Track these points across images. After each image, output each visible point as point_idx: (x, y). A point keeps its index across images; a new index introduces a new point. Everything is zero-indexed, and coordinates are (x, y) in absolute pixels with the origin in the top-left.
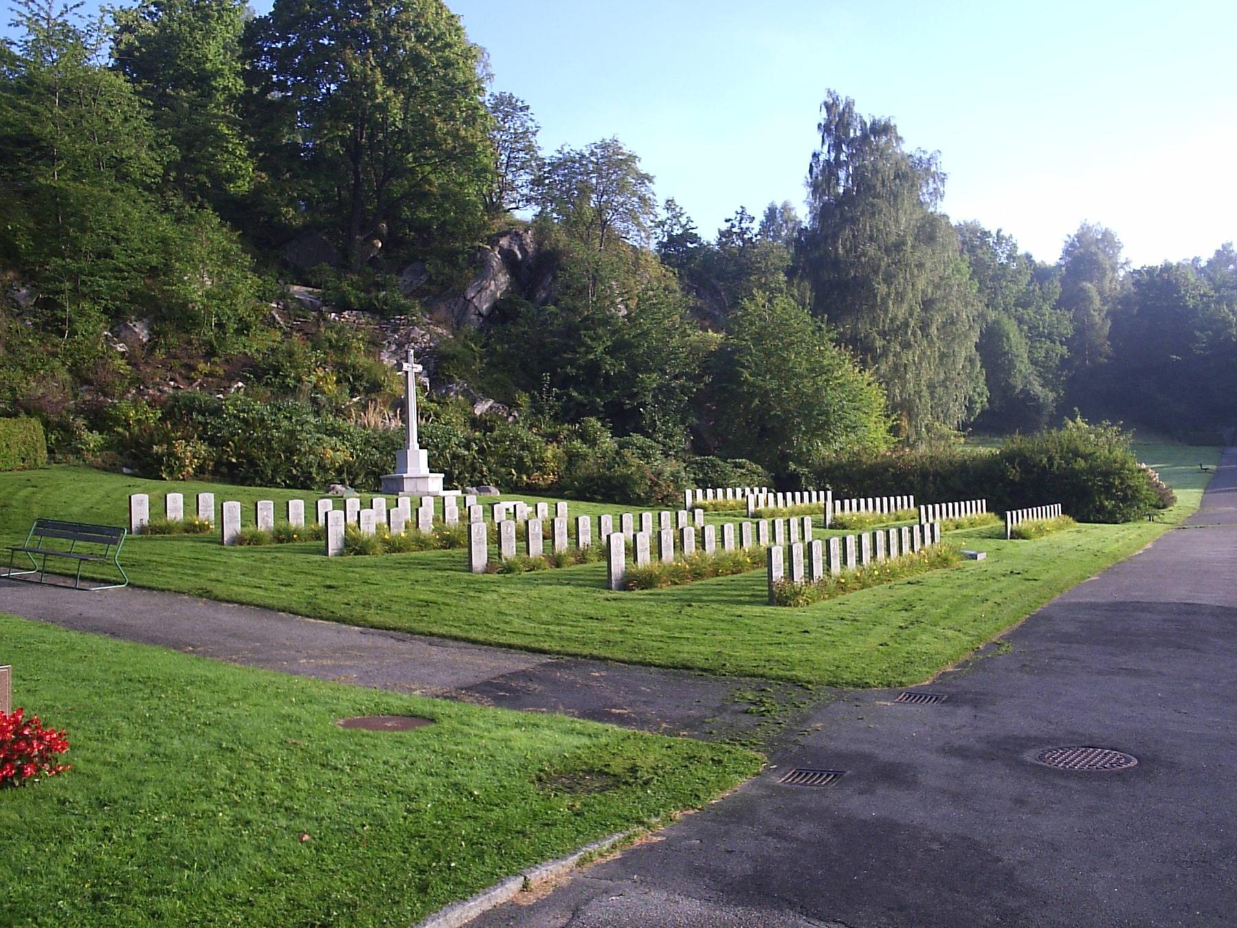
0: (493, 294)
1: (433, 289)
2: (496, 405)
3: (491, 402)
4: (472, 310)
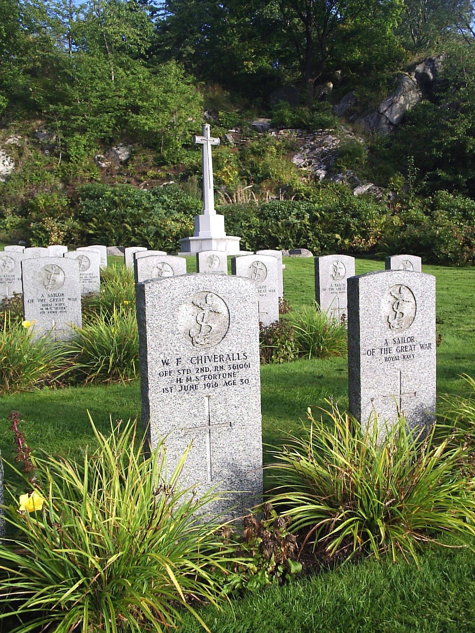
0: (403, 106)
1: (358, 108)
2: (374, 188)
3: (370, 185)
4: (384, 120)
